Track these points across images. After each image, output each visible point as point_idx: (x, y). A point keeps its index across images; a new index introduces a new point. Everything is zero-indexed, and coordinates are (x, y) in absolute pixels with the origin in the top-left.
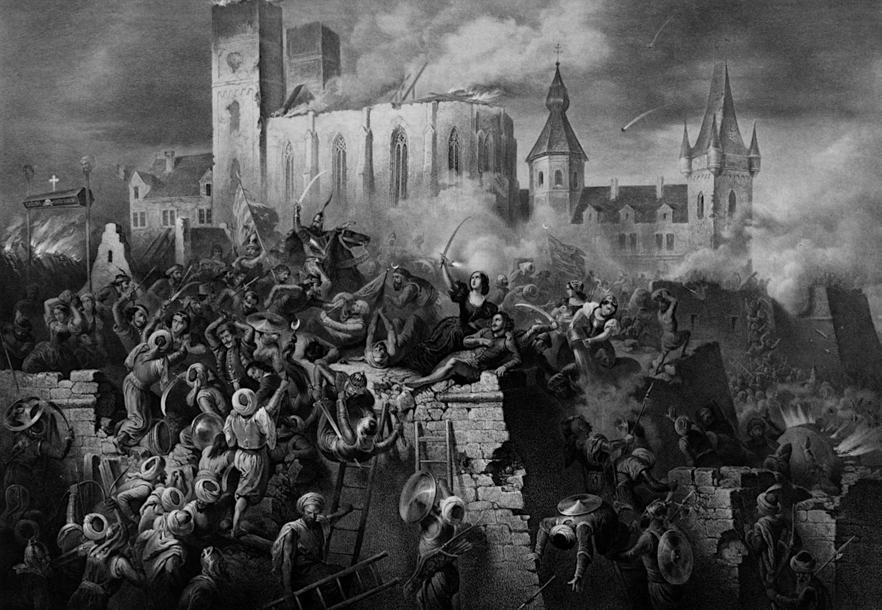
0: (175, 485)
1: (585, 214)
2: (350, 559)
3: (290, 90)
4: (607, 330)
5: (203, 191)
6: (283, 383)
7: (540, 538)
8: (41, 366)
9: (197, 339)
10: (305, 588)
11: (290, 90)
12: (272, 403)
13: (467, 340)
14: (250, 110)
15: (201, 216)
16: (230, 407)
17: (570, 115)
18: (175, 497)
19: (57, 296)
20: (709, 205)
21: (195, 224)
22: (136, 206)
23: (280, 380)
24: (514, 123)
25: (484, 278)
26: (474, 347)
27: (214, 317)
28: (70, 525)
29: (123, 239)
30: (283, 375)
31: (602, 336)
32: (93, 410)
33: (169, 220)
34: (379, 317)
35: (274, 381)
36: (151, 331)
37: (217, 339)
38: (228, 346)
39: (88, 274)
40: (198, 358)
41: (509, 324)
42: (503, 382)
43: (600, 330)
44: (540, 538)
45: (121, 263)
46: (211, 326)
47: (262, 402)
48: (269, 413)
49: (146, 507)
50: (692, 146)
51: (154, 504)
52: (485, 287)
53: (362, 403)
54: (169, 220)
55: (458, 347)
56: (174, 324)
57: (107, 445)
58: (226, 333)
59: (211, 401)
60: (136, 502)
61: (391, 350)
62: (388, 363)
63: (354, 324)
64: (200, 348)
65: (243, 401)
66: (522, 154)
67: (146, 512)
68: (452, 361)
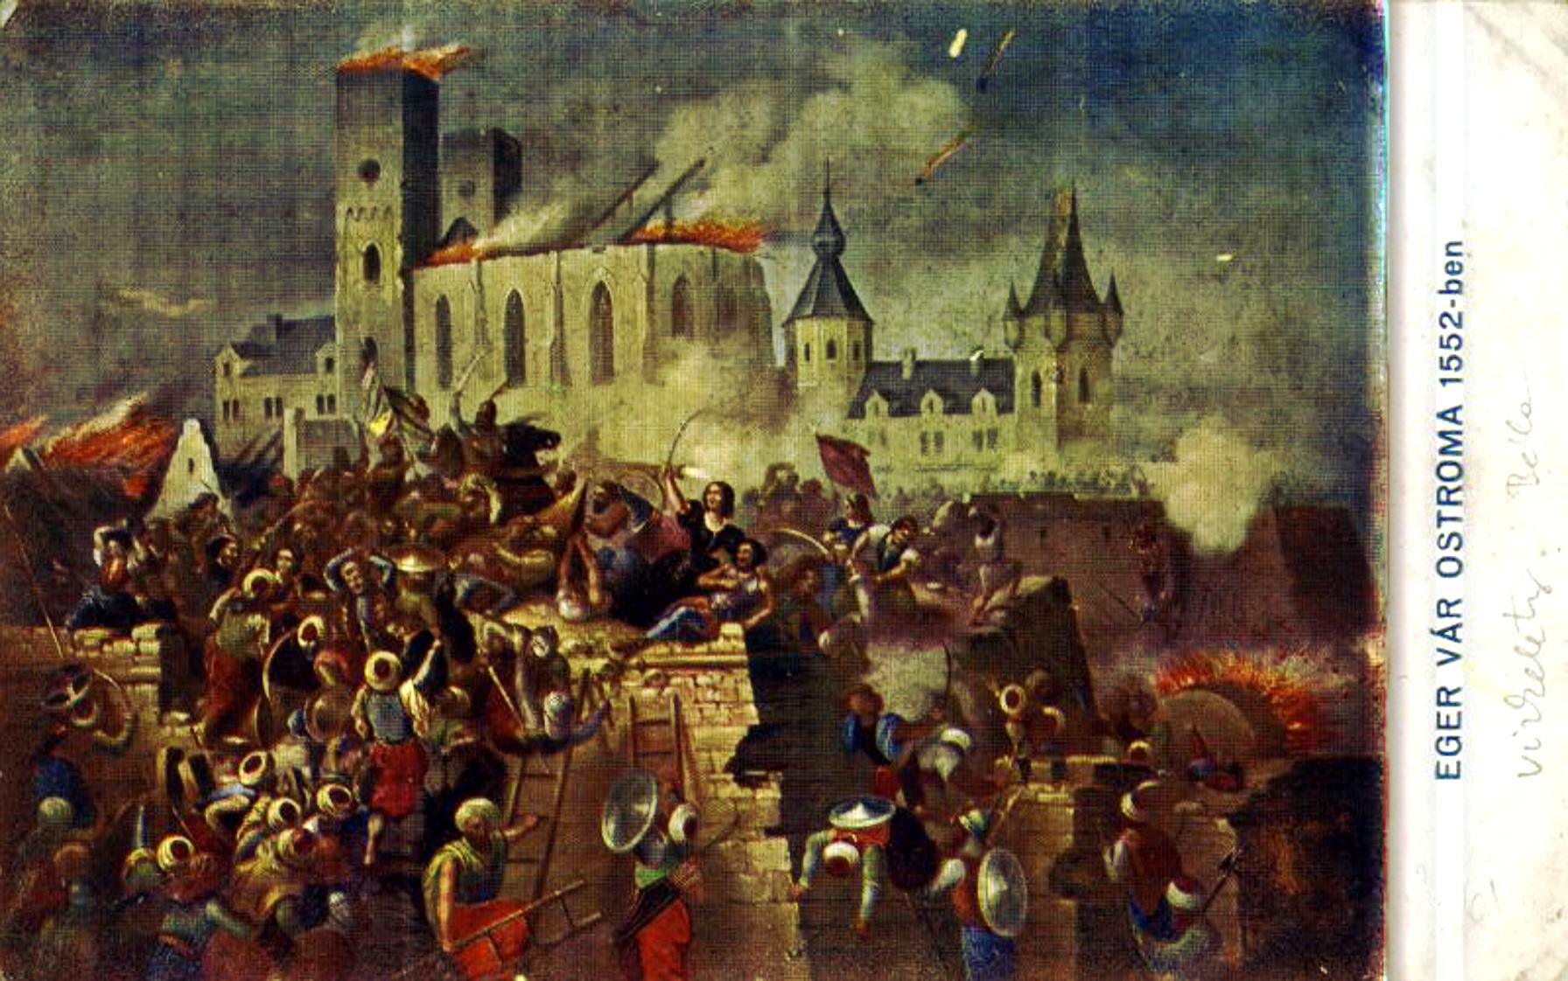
2: (530, 891)
4: (903, 565)
5: (321, 369)
7: (808, 861)
8: (90, 618)
11: (446, 224)
12: (424, 670)
13: (703, 580)
14: (393, 255)
16: (360, 679)
17: (844, 260)
18: (286, 811)
29: (209, 439)
31: (896, 571)
32: (746, 671)
33: (274, 410)
34: (575, 548)
37: (340, 581)
40: (317, 609)
42: (751, 636)
43: (895, 561)
44: (808, 861)
45: (206, 478)
46: (332, 562)
47: (408, 670)
48: (418, 688)
51: (255, 825)
54: (274, 410)
55: (689, 588)
56: (280, 563)
59: (334, 669)
60: (232, 820)
62: (591, 616)
63: (537, 559)
67: (245, 838)
68: (682, 610)
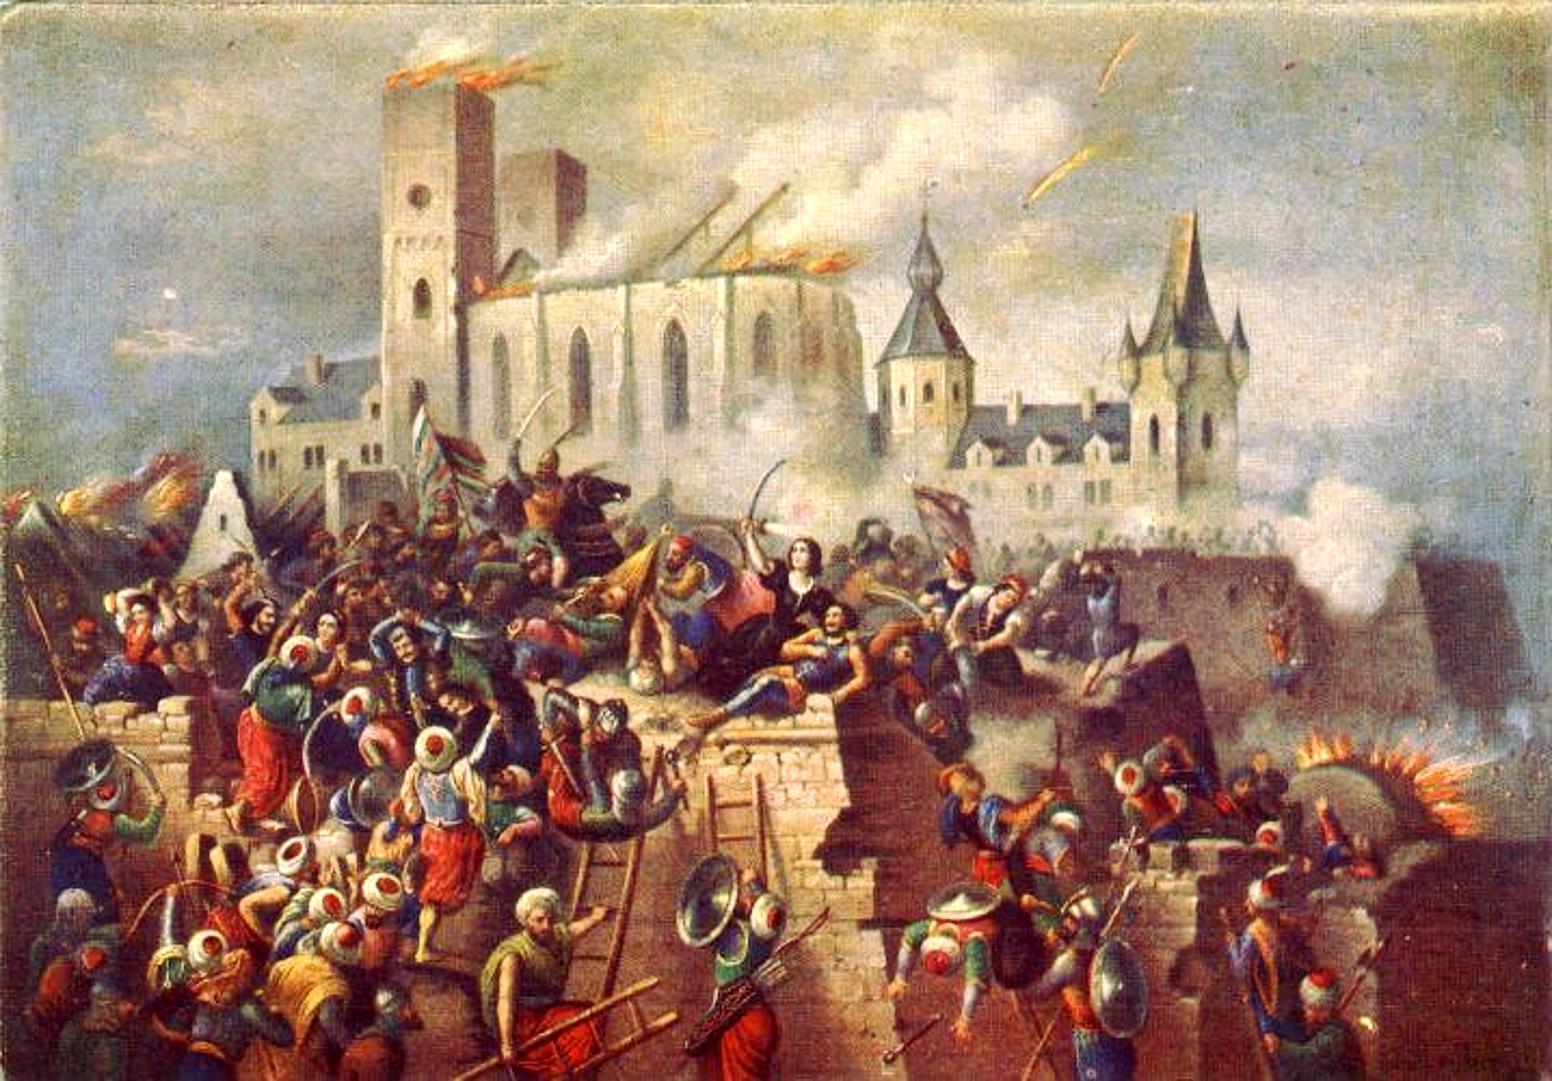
0: (332, 884)
1: (970, 454)
3: (504, 253)
6: (495, 718)
8: (109, 693)
9: (358, 651)
10: (756, 688)
11: (504, 253)
12: (480, 749)
15: (364, 452)
16: (410, 756)
17: (944, 295)
19: (138, 587)
20: (1169, 433)
21: (356, 465)
22: (261, 440)
23: (487, 713)
24: (857, 311)
25: (814, 549)
26: (796, 661)
27: (387, 612)
28: (167, 950)
30: (492, 704)
34: (648, 617)
35: (480, 716)
36: (282, 640)
38: (407, 660)
39: (275, 640)
41: (851, 620)
49: (284, 924)
50: (1140, 341)
52: (814, 568)
53: (620, 748)
56: (321, 629)
57: (212, 815)
58: (405, 640)
61: (668, 665)
62: (664, 687)
64: (363, 665)
65: (435, 747)
66: (871, 353)
